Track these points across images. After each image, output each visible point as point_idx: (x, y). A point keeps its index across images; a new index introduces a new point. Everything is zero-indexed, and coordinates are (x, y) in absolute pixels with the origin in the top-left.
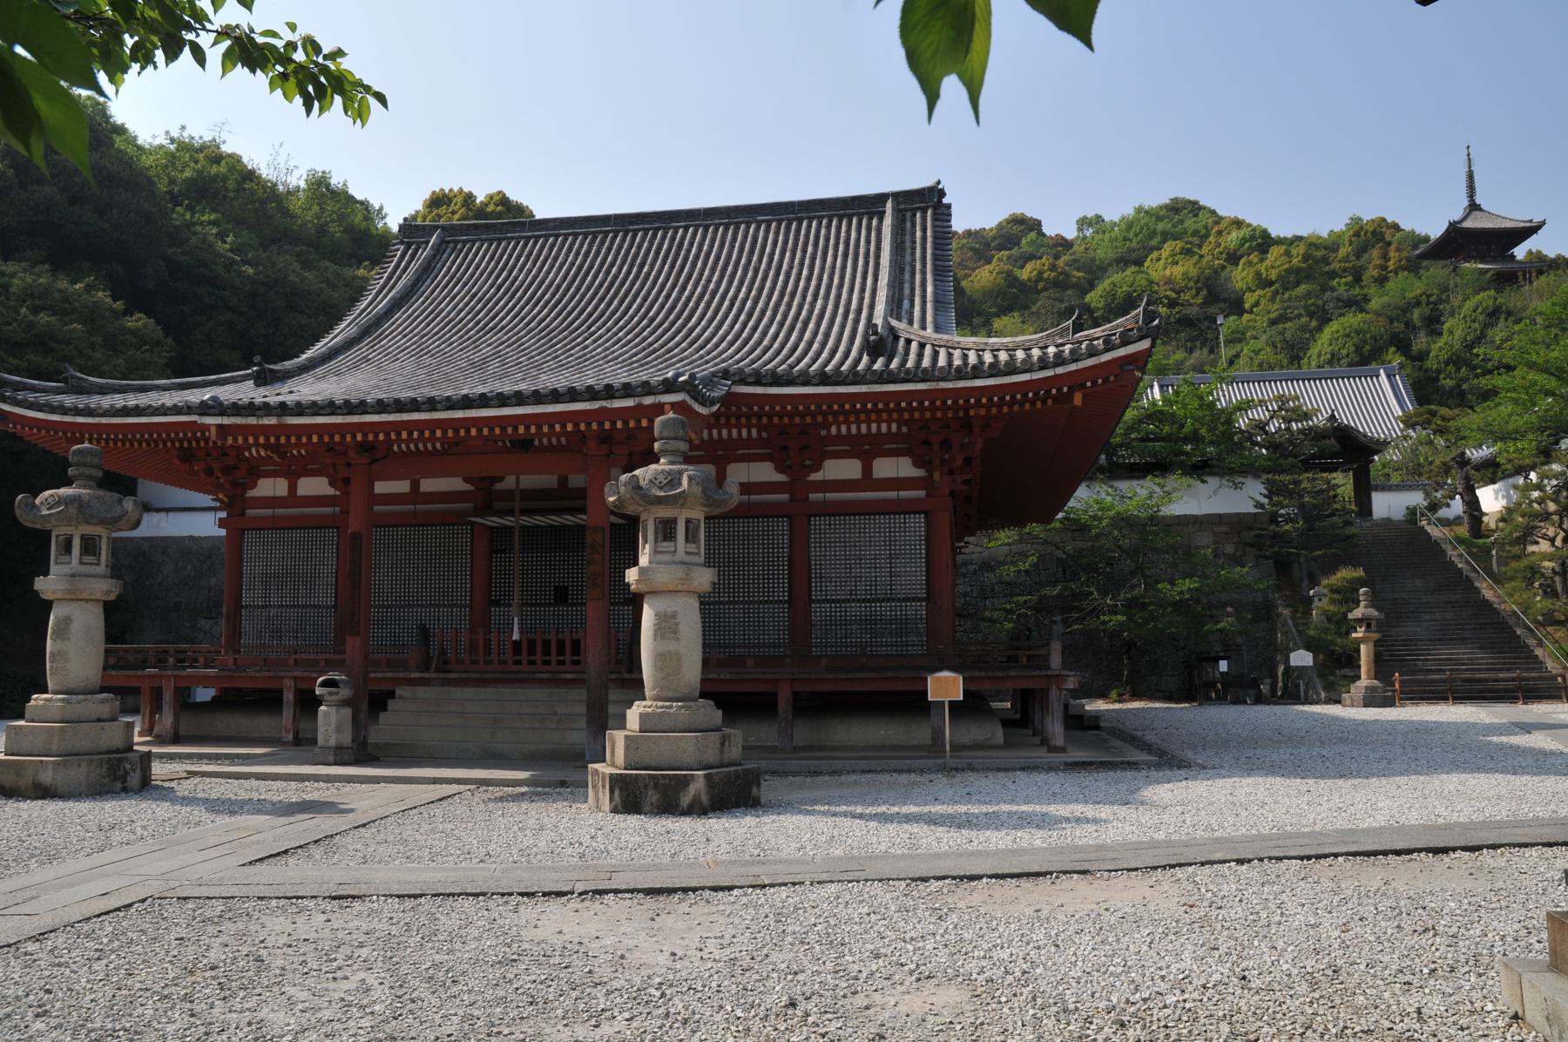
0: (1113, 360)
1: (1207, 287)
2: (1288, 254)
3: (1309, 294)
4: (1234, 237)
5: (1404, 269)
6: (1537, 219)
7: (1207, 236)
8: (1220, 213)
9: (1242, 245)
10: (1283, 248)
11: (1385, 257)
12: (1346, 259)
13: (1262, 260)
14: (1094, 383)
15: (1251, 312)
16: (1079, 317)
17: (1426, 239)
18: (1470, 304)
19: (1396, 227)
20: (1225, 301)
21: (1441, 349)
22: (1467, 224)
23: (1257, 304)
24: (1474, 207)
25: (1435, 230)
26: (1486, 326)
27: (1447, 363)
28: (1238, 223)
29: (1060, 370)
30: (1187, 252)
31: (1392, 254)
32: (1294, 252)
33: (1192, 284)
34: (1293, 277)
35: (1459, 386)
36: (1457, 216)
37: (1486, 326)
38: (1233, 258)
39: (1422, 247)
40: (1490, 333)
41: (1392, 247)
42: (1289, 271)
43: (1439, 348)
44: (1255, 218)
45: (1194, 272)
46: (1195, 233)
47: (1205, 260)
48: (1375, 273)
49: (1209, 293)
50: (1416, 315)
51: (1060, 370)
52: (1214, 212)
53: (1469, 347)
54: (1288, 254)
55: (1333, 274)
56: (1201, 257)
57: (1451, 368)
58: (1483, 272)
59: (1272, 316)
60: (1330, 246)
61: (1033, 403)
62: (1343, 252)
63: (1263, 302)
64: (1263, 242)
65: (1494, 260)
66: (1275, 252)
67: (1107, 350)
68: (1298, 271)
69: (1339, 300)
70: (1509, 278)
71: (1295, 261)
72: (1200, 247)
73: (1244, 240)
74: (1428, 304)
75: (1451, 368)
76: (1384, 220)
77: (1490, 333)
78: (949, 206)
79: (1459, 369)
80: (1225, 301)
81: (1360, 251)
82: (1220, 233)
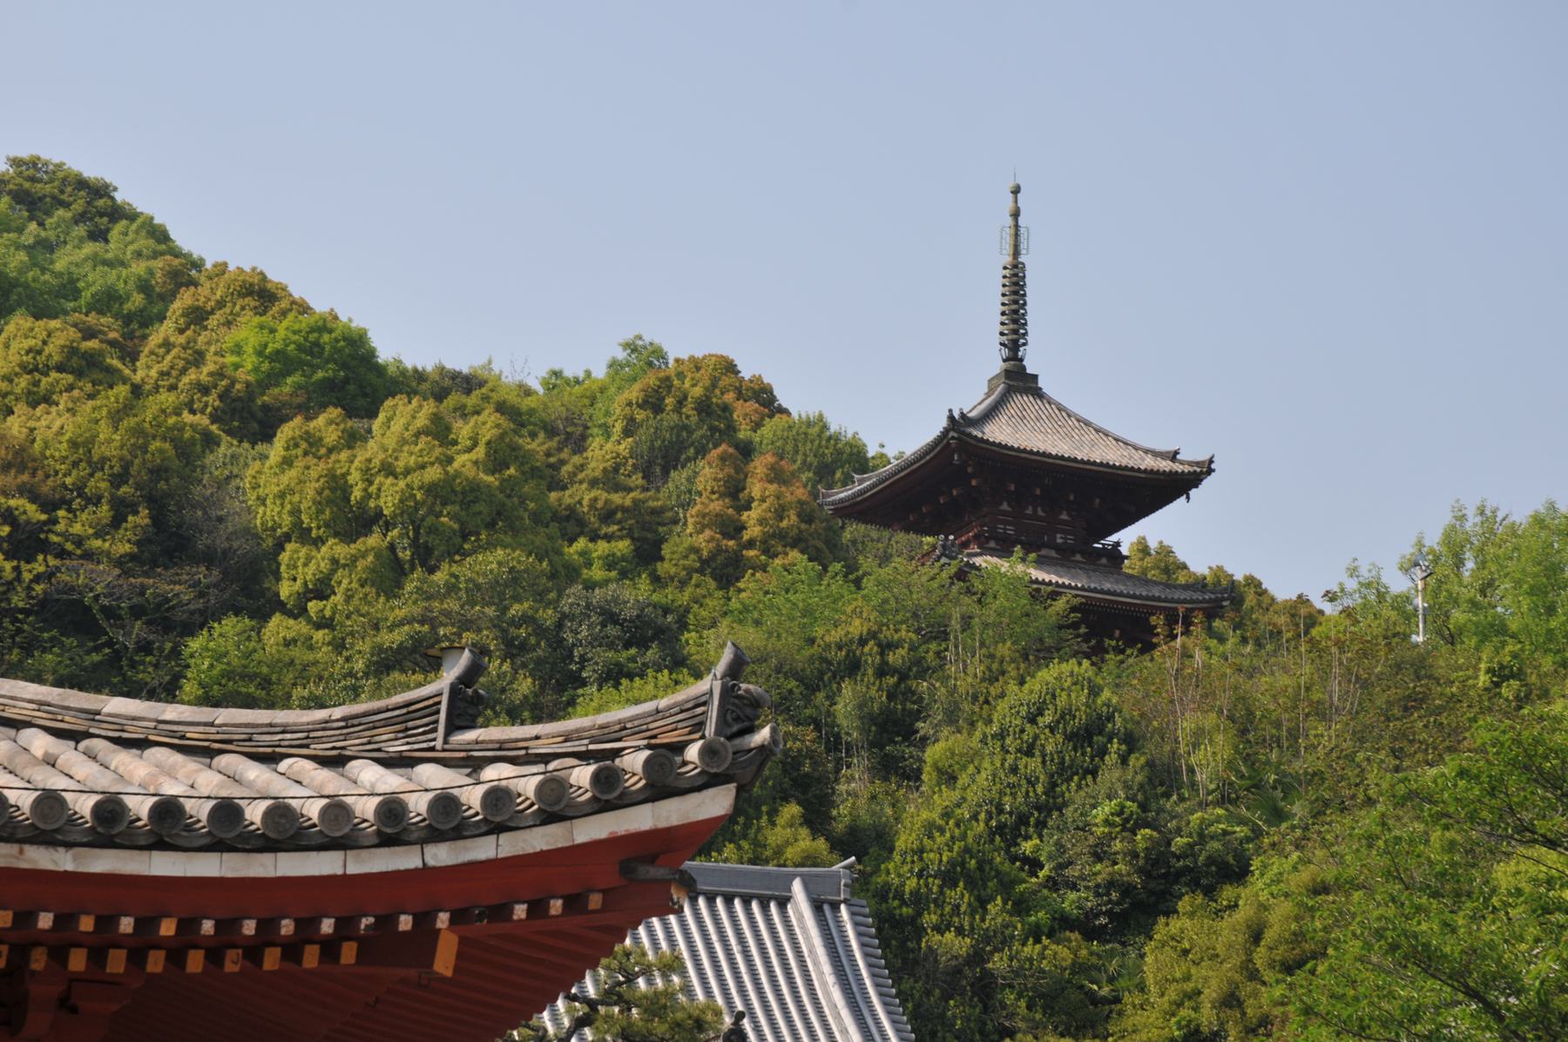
0: (613, 842)
1: (156, 503)
2: (439, 431)
3: (515, 581)
4: (241, 345)
5: (797, 542)
6: (1192, 453)
7: (146, 320)
8: (186, 238)
9: (270, 380)
10: (422, 412)
11: (734, 490)
12: (611, 479)
13: (353, 439)
14: (537, 908)
15: (299, 612)
16: (468, 678)
17: (854, 458)
18: (1014, 698)
19: (763, 397)
20: (209, 558)
21: (930, 829)
22: (999, 432)
23: (321, 590)
24: (1018, 381)
25: (898, 432)
26: (1064, 772)
27: (949, 878)
28: (261, 294)
29: (441, 855)
30: (85, 367)
31: (755, 488)
32: (462, 430)
33: (99, 484)
34: (441, 525)
35: (977, 957)
36: (970, 397)
37: (1064, 772)
38: (251, 418)
39: (861, 485)
40: (1074, 793)
41: (760, 465)
42: (440, 493)
43: (924, 821)
44: (328, 287)
45: (111, 442)
46: (108, 301)
47: (151, 408)
48: (704, 541)
49: (157, 520)
50: (846, 705)
51: (441, 855)
52: (160, 235)
53: (1010, 832)
54: (439, 431)
55: (572, 524)
56: (137, 390)
57: (959, 895)
58: (1041, 595)
59: (392, 639)
60: (558, 420)
61: (253, 951)
62: (600, 452)
63: (344, 582)
64: (349, 377)
65: (1063, 558)
66: (398, 420)
67: (601, 805)
68: (470, 494)
69: (610, 617)
70: (1121, 623)
71: (461, 461)
72: (131, 357)
73: (281, 363)
74: (881, 672)
75: (959, 895)
76: (730, 368)
77: (1074, 793)
78: (254, 269)
79: (982, 903)
80: (209, 558)
81: (663, 460)
82: (197, 316)
